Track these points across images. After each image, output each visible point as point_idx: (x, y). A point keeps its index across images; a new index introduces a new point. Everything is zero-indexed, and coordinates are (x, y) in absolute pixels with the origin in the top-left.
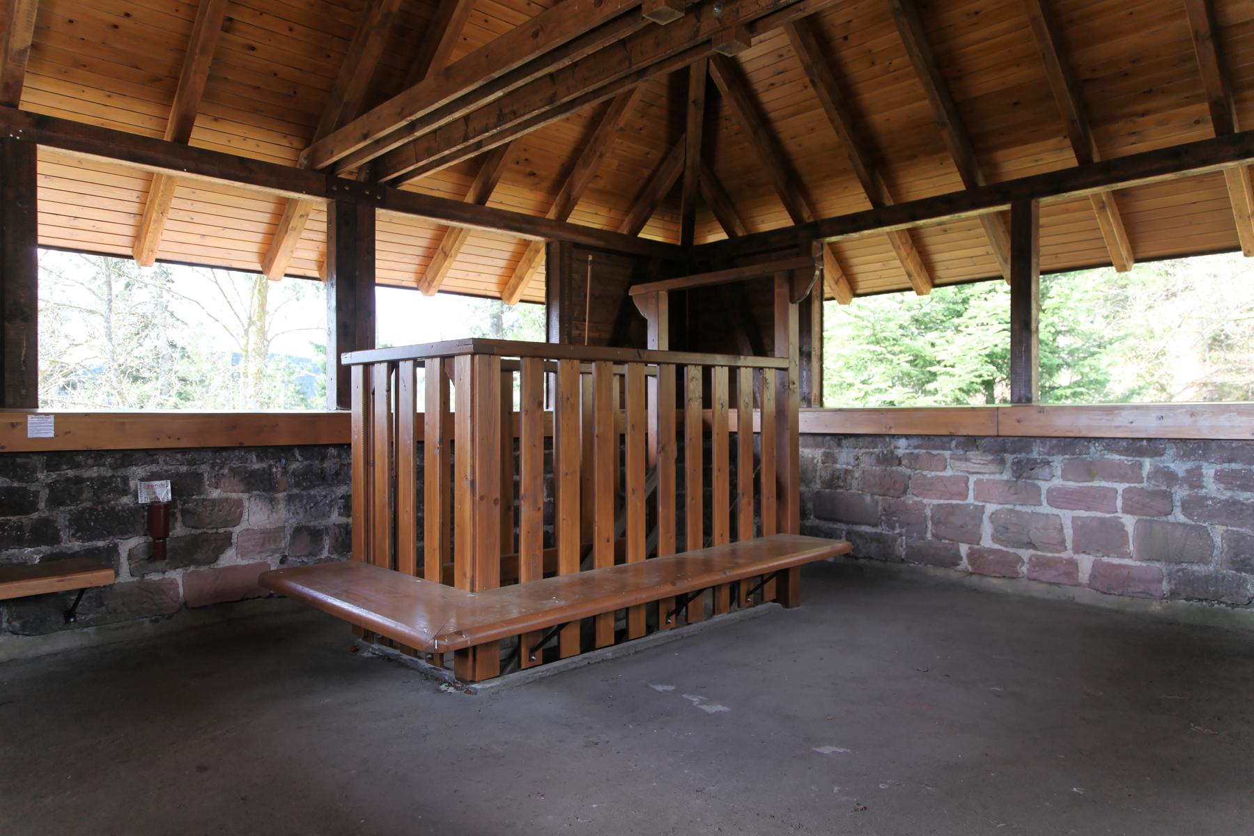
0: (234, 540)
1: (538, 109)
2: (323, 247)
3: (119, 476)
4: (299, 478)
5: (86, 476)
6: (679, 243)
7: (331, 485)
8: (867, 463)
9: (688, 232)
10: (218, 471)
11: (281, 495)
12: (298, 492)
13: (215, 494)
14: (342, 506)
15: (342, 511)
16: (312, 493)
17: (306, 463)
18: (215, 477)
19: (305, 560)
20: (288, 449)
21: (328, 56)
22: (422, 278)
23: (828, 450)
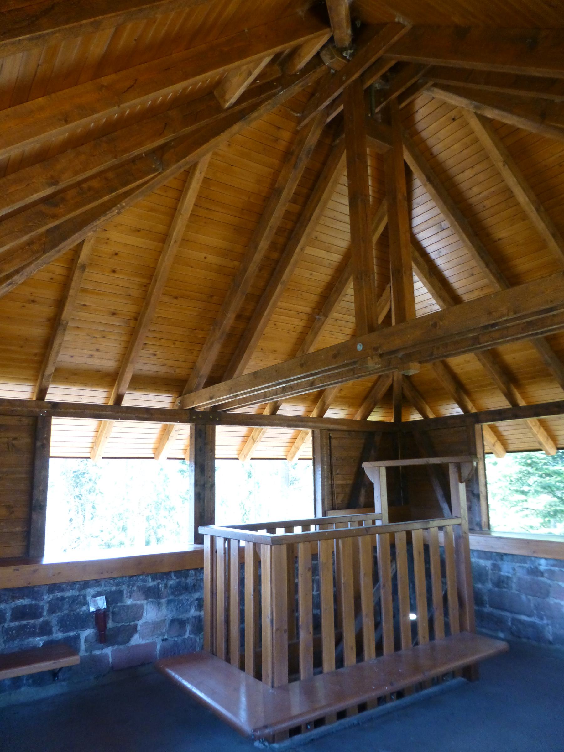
0: (138, 628)
1: (304, 388)
2: (187, 443)
3: (82, 595)
4: (173, 590)
5: (66, 596)
6: (393, 421)
7: (190, 593)
8: (521, 573)
9: (398, 415)
10: (131, 588)
11: (164, 601)
12: (173, 598)
13: (129, 602)
14: (197, 605)
15: (197, 608)
16: (181, 598)
17: (178, 580)
18: (129, 592)
19: (176, 639)
20: (168, 574)
21: (192, 353)
22: (240, 452)
23: (495, 562)
